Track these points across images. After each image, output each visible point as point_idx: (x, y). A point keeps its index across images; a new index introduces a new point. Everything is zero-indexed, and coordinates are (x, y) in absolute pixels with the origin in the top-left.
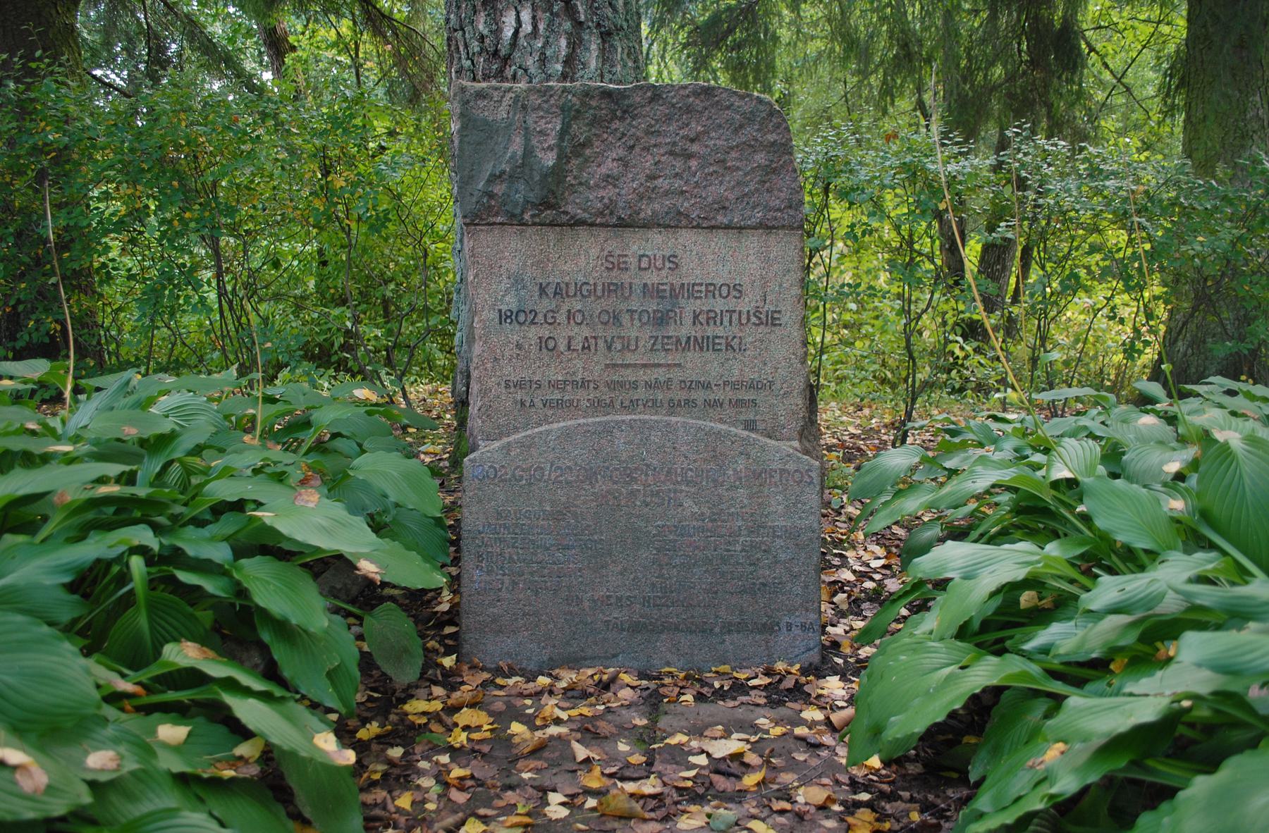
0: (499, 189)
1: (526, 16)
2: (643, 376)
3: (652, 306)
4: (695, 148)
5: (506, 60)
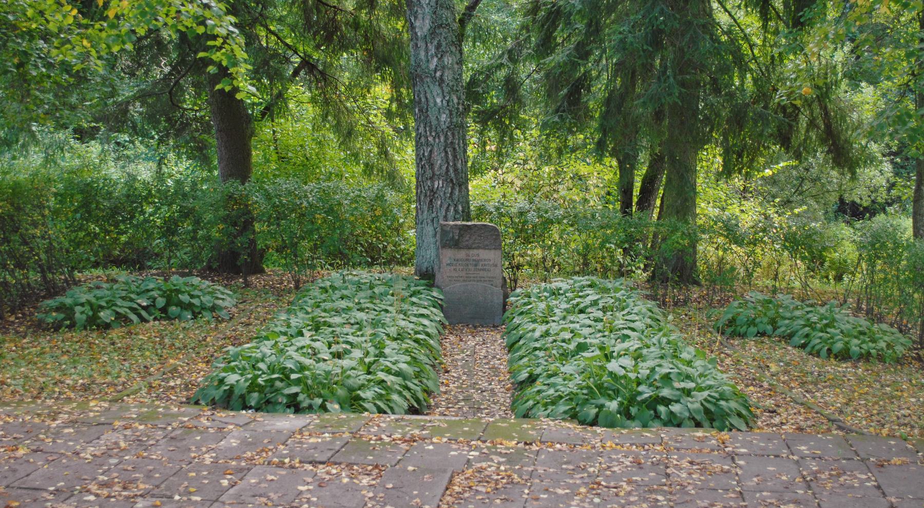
1: (441, 182)
2: (472, 276)
5: (435, 193)
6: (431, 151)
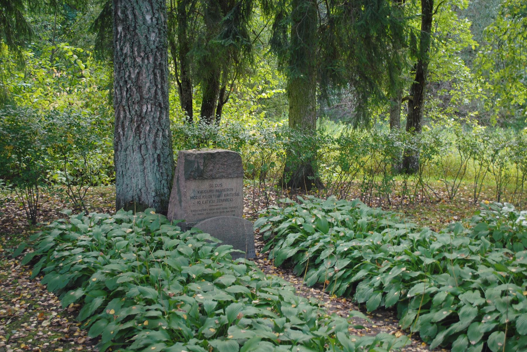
0: (192, 174)
1: (149, 106)
2: (215, 207)
3: (217, 194)
4: (225, 163)
6: (138, 73)
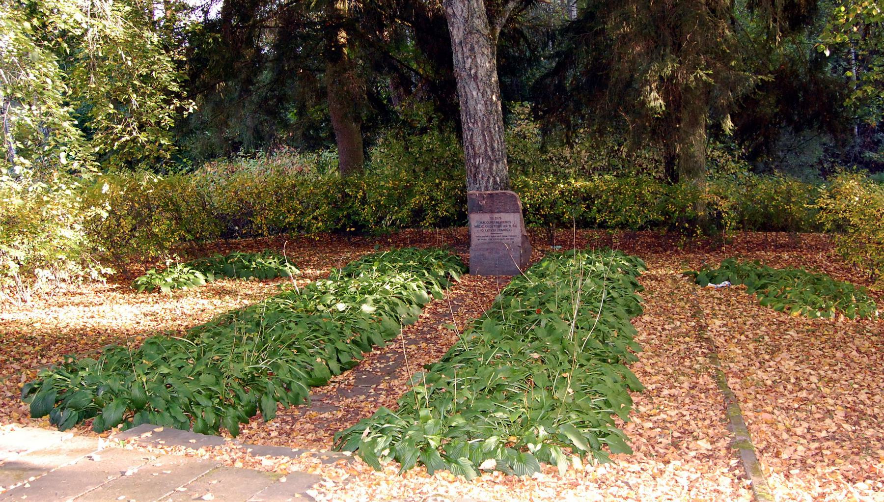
1: (481, 159)
